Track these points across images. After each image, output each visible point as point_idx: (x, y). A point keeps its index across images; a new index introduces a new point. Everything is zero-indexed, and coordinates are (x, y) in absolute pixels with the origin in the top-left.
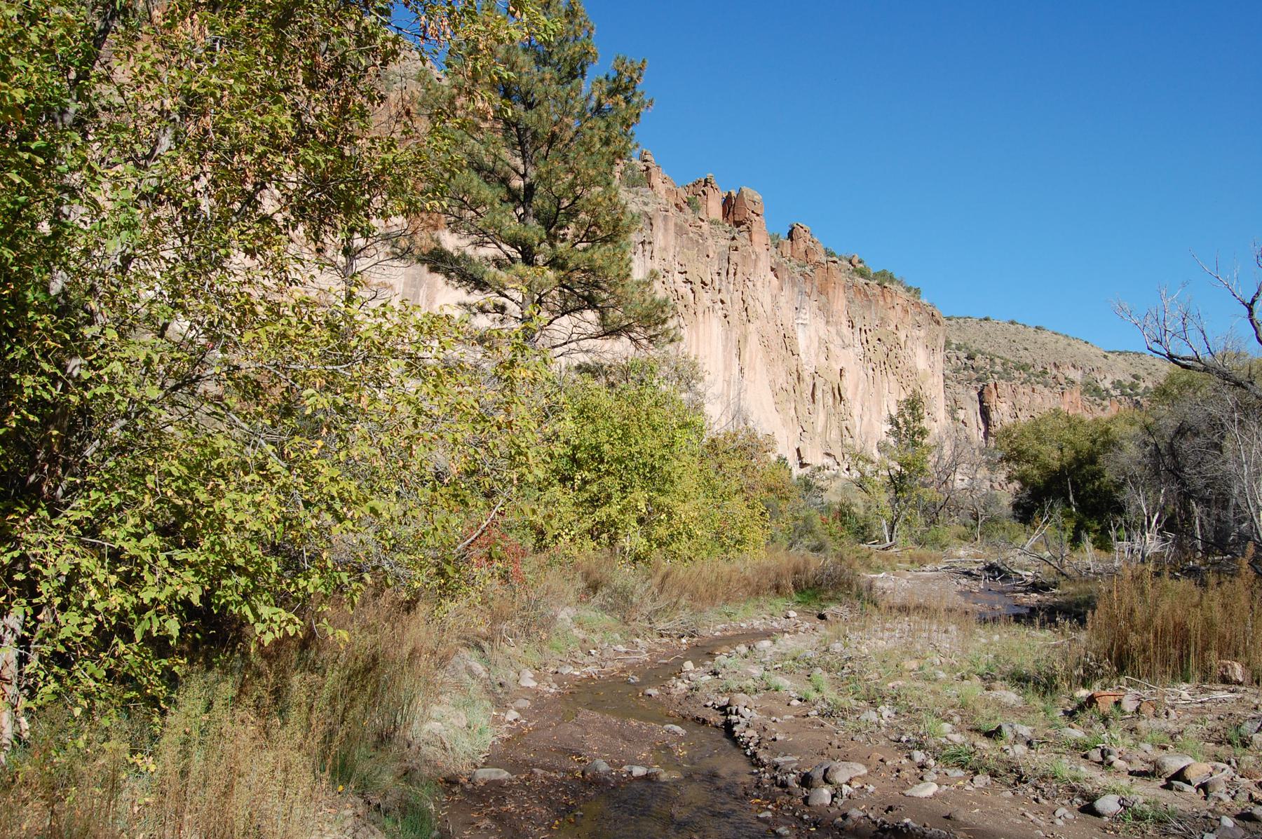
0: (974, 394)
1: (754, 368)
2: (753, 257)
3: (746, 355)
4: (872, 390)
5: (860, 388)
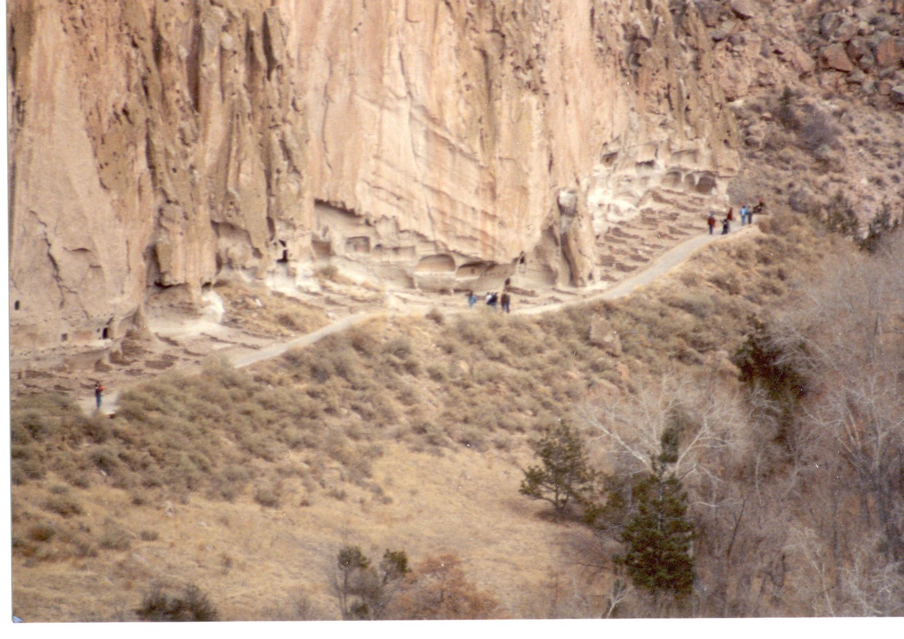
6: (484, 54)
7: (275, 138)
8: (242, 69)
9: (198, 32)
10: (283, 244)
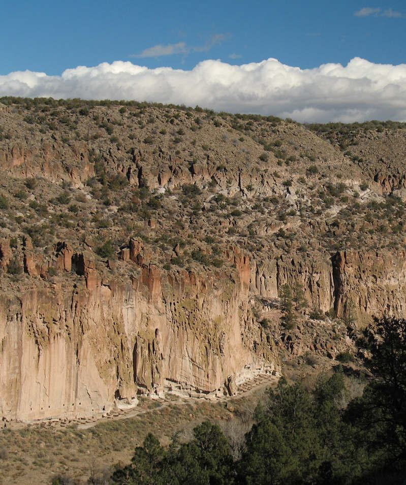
0: (328, 257)
1: (86, 359)
2: (87, 296)
3: (81, 353)
4: (177, 340)
5: (169, 338)
6: (206, 348)
7: (154, 366)
8: (147, 351)
9: (136, 345)
10: (156, 388)
